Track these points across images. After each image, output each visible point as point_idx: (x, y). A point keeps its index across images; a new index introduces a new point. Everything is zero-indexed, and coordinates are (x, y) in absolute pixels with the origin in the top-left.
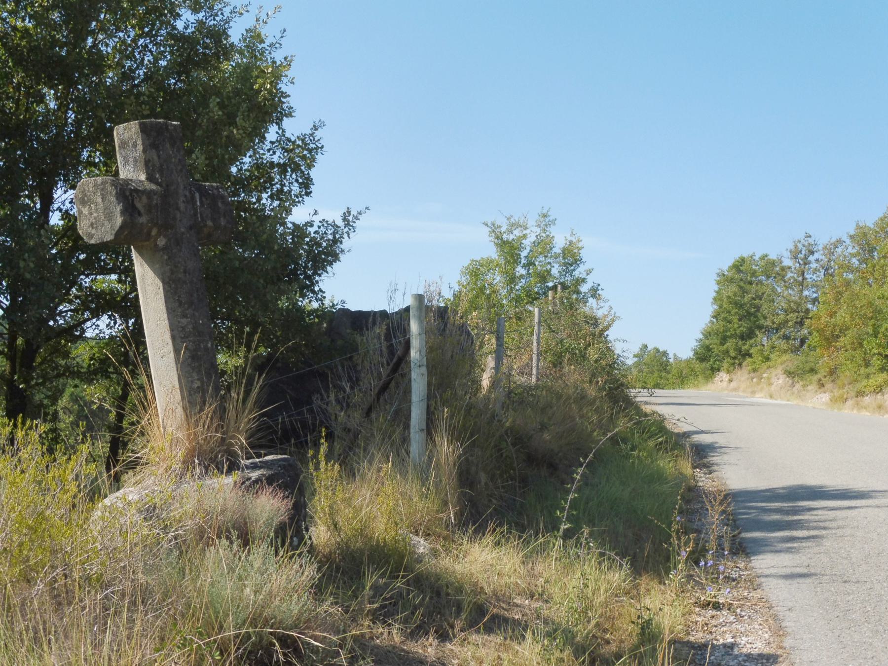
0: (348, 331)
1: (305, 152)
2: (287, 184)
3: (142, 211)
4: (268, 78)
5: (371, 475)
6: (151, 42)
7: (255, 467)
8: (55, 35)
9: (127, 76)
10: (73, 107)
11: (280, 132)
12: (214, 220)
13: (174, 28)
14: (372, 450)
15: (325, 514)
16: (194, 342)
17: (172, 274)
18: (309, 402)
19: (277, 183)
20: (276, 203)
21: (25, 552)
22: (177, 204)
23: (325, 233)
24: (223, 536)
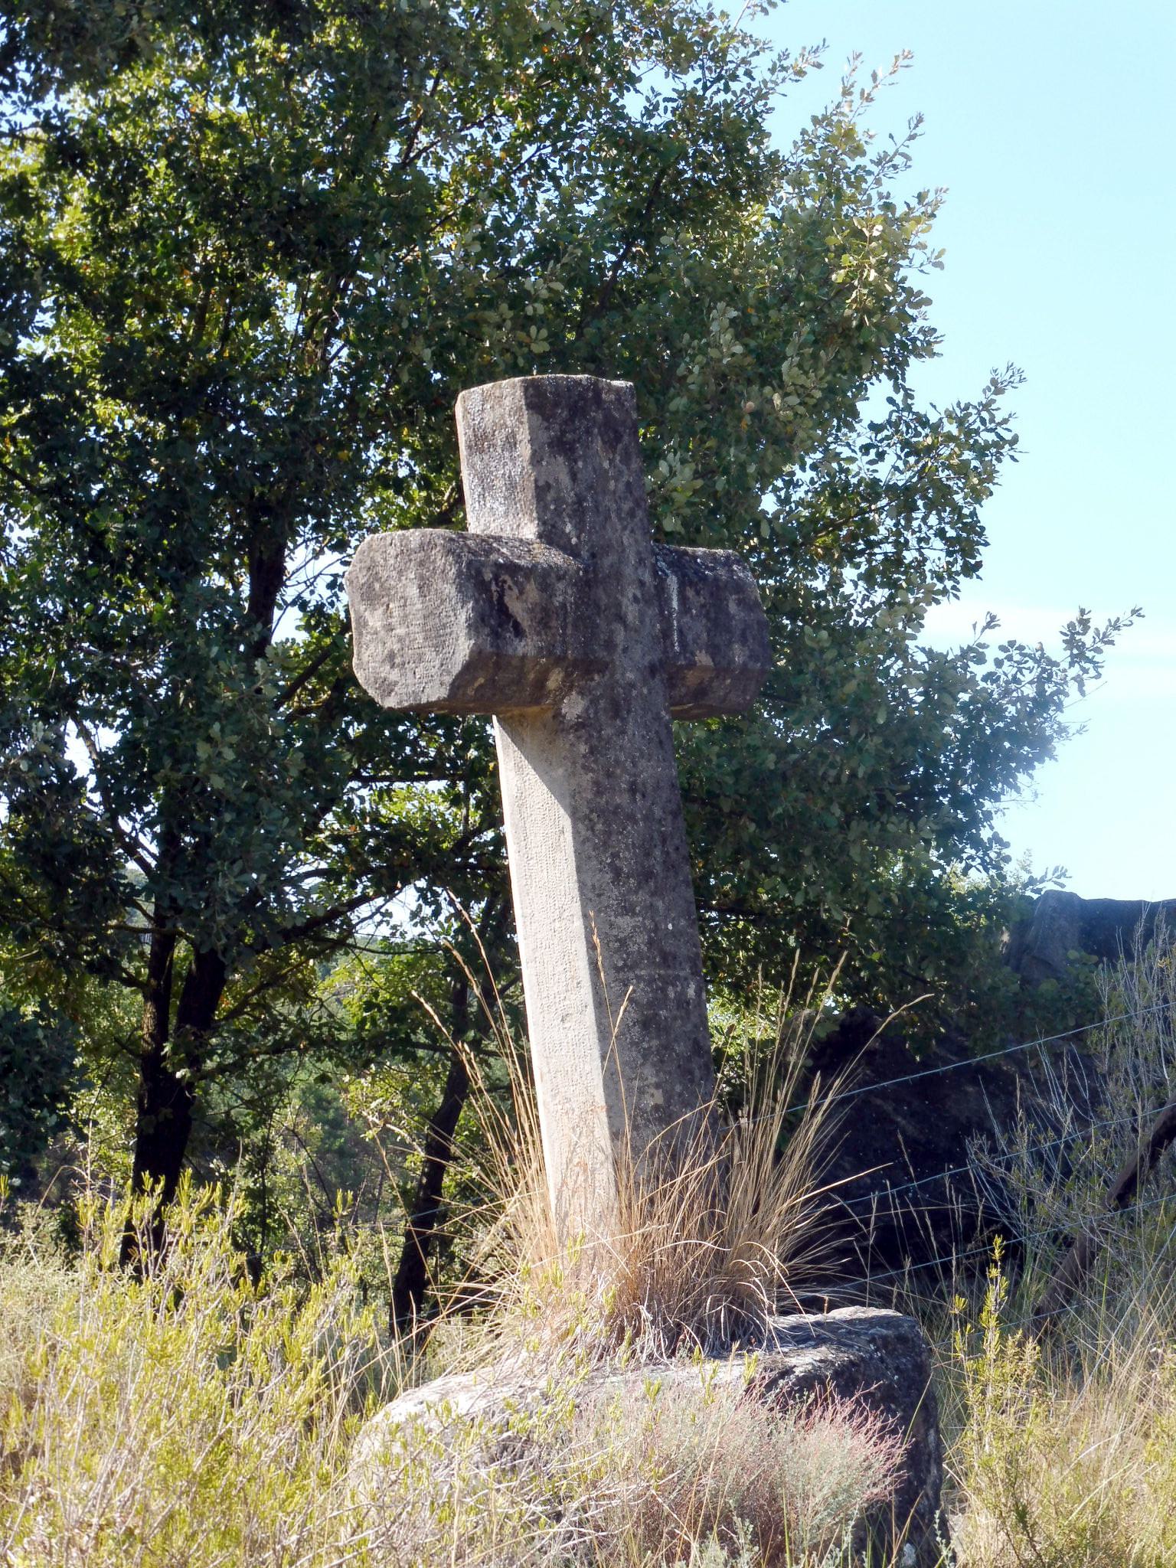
0: (1073, 954)
1: (967, 455)
2: (913, 542)
3: (525, 623)
4: (872, 252)
5: (1129, 1373)
6: (555, 153)
7: (801, 1338)
8: (305, 138)
9: (492, 245)
10: (345, 329)
11: (899, 398)
12: (713, 650)
13: (619, 114)
14: (1135, 1300)
15: (992, 1483)
16: (650, 982)
17: (599, 793)
18: (960, 1158)
19: (885, 540)
20: (880, 595)
21: (178, 1541)
22: (619, 605)
23: (1015, 680)
24: (713, 1536)
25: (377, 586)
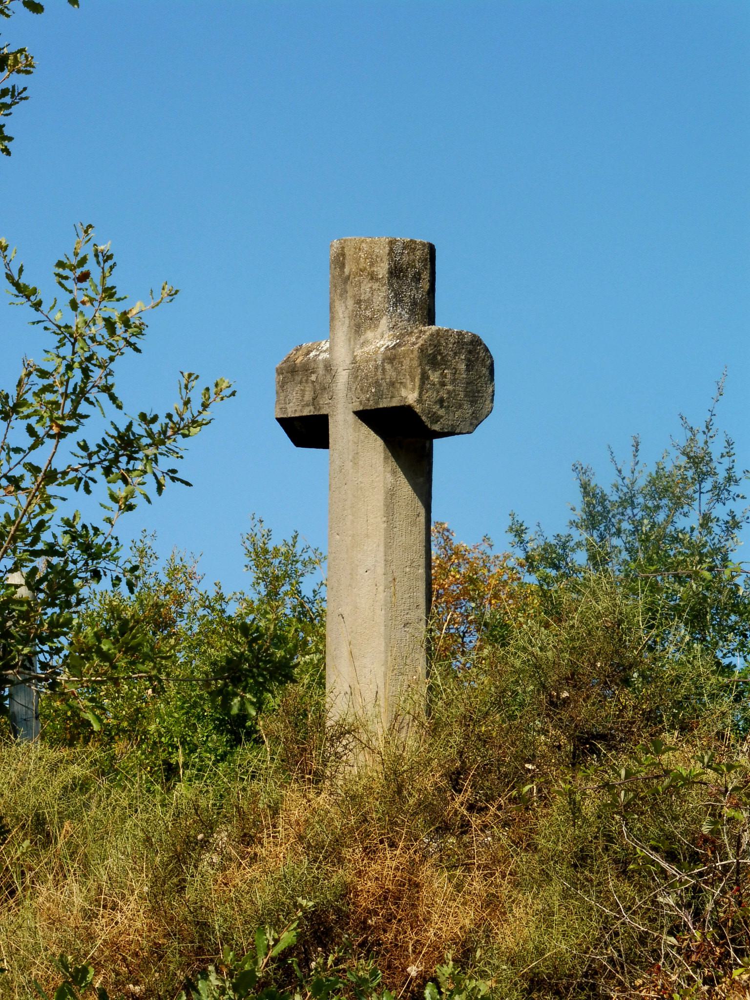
25: (439, 358)
